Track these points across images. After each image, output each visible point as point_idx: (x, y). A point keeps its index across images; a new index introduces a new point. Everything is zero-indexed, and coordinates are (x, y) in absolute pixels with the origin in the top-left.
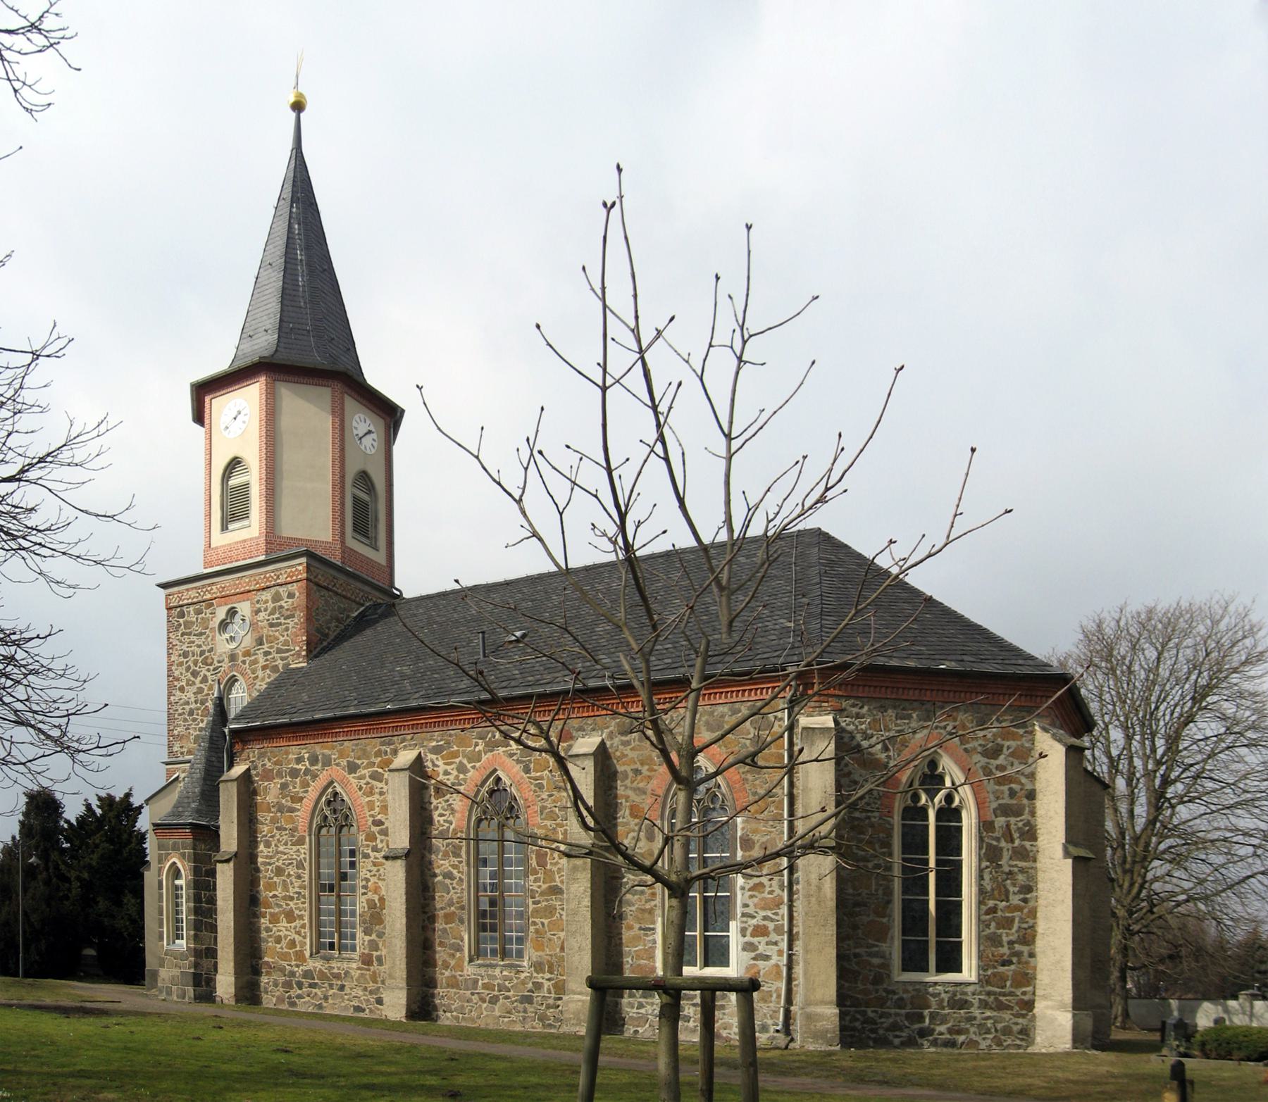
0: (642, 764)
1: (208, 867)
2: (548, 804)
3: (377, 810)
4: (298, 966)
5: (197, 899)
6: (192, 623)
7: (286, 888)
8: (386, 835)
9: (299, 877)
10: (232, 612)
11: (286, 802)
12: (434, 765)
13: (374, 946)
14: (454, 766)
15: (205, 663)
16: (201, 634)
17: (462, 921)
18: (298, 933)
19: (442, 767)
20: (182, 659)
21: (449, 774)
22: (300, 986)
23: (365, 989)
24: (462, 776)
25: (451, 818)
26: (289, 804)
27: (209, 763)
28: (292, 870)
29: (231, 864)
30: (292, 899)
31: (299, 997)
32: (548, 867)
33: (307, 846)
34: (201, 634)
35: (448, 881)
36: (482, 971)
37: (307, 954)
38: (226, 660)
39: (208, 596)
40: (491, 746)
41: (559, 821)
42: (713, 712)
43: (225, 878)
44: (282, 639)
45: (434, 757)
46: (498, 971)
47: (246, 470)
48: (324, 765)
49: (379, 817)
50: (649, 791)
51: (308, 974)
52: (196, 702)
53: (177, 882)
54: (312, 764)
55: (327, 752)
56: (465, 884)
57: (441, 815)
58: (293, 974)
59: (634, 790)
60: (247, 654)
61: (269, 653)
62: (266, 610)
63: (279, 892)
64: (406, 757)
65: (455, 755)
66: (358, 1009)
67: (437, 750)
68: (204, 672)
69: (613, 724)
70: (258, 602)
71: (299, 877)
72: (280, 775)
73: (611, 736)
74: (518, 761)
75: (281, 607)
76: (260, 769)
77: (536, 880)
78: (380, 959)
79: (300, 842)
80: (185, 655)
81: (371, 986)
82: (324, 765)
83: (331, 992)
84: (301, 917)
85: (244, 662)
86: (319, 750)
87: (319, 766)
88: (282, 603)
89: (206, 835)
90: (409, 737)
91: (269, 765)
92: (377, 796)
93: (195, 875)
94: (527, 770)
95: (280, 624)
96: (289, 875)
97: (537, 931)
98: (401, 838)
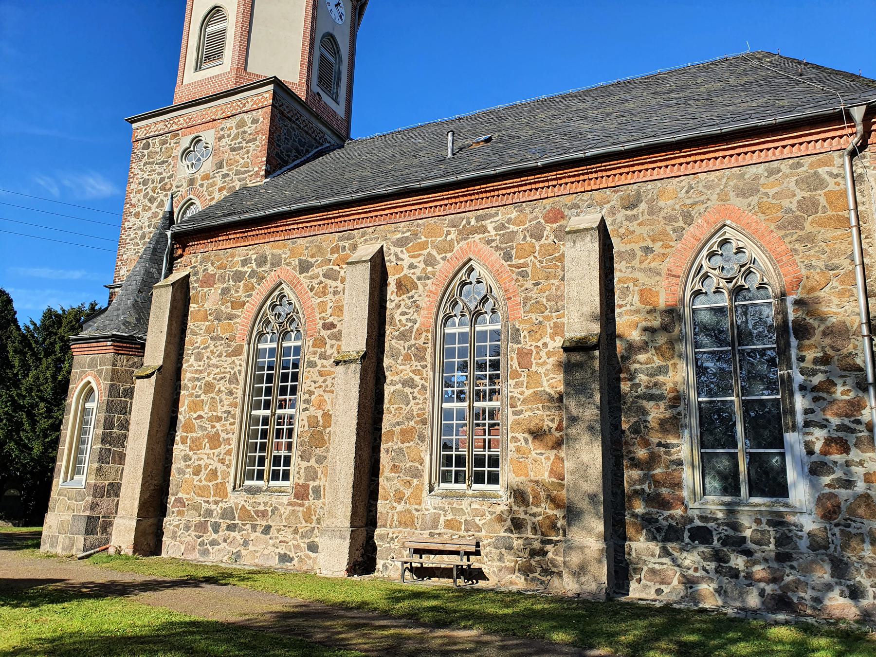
0: (653, 241)
1: (128, 386)
2: (533, 294)
3: (329, 311)
4: (216, 503)
5: (108, 424)
6: (156, 153)
7: (213, 408)
8: (338, 339)
9: (231, 393)
10: (197, 141)
11: (226, 309)
12: (398, 258)
13: (312, 474)
14: (422, 258)
15: (163, 189)
16: (163, 162)
17: (422, 438)
18: (222, 461)
19: (407, 260)
20: (141, 187)
21: (416, 267)
22: (216, 528)
23: (296, 531)
24: (430, 269)
25: (415, 316)
26: (229, 310)
27: (147, 272)
28: (222, 386)
29: (153, 378)
30: (219, 419)
31: (214, 543)
32: (534, 368)
33: (244, 357)
34: (163, 162)
35: (408, 390)
36: (445, 503)
37: (230, 487)
38: (185, 184)
39: (175, 127)
40: (466, 233)
41: (547, 313)
42: (742, 175)
43: (144, 395)
44: (242, 161)
45: (398, 250)
46: (465, 503)
47: (224, 18)
48: (273, 265)
49: (331, 319)
50: (664, 271)
51: (227, 514)
52: (149, 226)
53: (88, 405)
54: (259, 265)
55: (277, 251)
56: (429, 392)
57: (404, 314)
58: (209, 513)
59: (645, 270)
60: (206, 177)
61: (228, 175)
62: (229, 136)
63: (206, 412)
64: (367, 251)
65: (423, 246)
66: (284, 558)
67: (401, 243)
68: (162, 197)
69: (615, 198)
70: (222, 129)
71: (231, 393)
72: (222, 279)
73: (613, 211)
74: (497, 248)
75: (245, 132)
76: (201, 275)
77: (517, 385)
78: (317, 491)
79: (237, 352)
80: (145, 182)
81: (303, 527)
82: (273, 265)
83: (253, 536)
84: (228, 441)
85: (202, 185)
86: (268, 250)
87: (267, 267)
88: (246, 129)
89: (131, 345)
90: (371, 230)
91: (211, 270)
92: (330, 296)
93: (110, 394)
94: (508, 257)
95: (242, 148)
96: (219, 391)
97: (518, 449)
98: (356, 341)
